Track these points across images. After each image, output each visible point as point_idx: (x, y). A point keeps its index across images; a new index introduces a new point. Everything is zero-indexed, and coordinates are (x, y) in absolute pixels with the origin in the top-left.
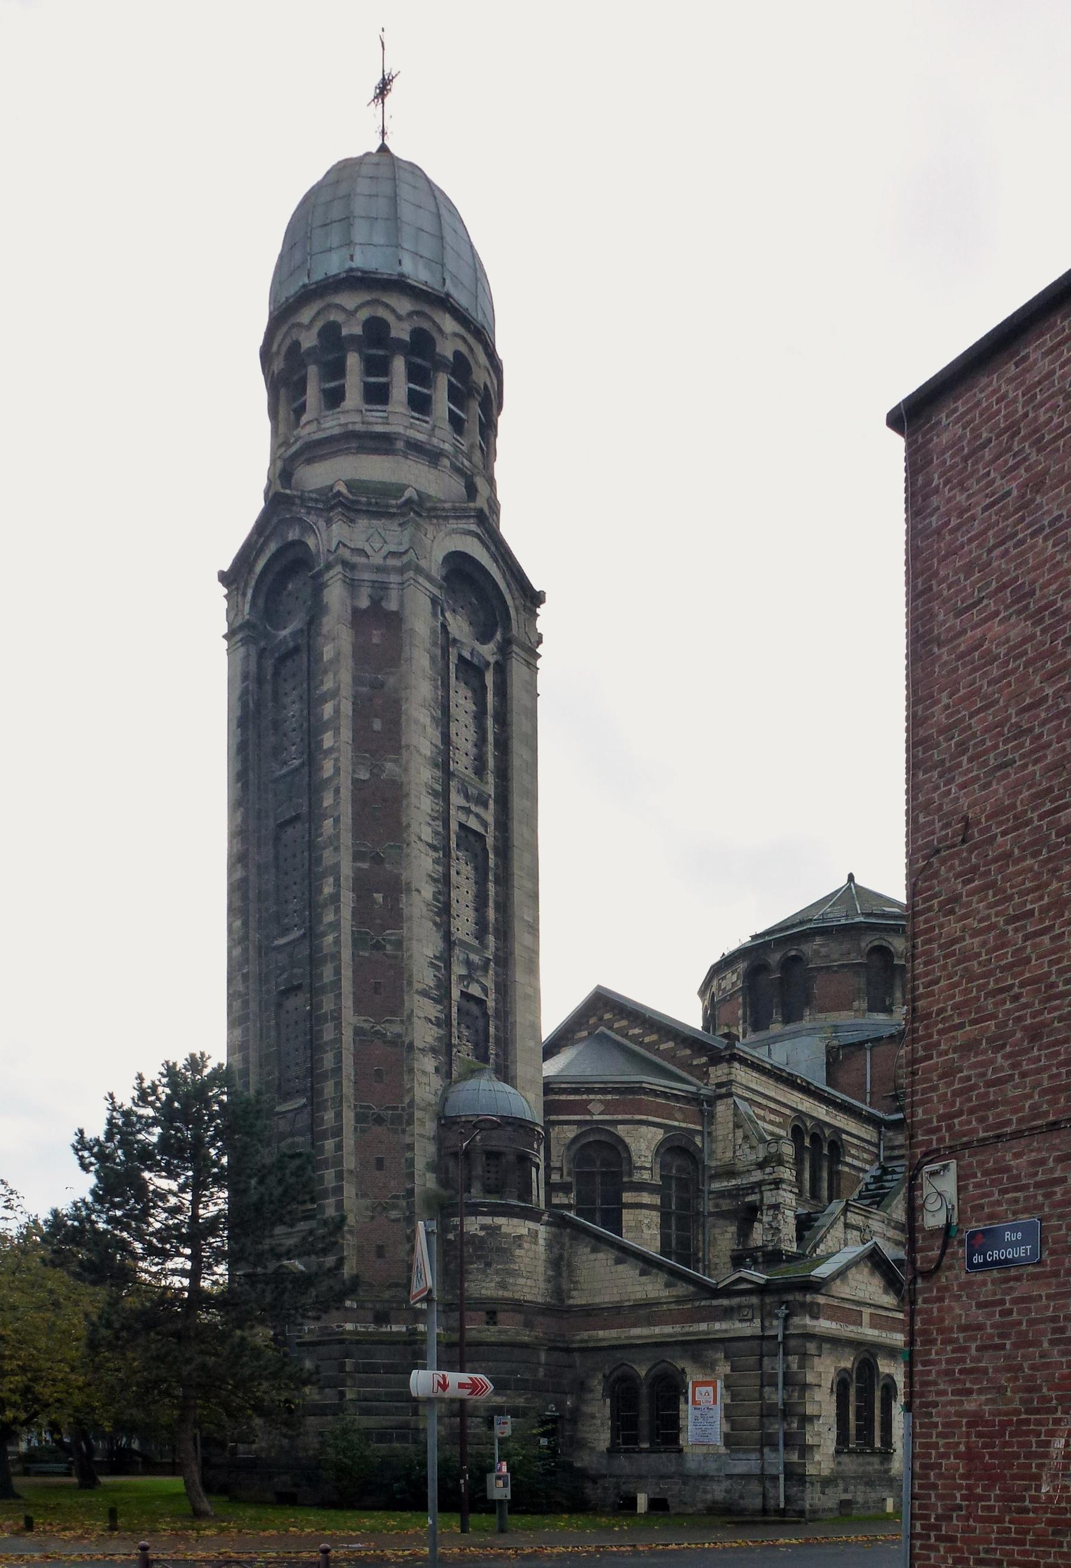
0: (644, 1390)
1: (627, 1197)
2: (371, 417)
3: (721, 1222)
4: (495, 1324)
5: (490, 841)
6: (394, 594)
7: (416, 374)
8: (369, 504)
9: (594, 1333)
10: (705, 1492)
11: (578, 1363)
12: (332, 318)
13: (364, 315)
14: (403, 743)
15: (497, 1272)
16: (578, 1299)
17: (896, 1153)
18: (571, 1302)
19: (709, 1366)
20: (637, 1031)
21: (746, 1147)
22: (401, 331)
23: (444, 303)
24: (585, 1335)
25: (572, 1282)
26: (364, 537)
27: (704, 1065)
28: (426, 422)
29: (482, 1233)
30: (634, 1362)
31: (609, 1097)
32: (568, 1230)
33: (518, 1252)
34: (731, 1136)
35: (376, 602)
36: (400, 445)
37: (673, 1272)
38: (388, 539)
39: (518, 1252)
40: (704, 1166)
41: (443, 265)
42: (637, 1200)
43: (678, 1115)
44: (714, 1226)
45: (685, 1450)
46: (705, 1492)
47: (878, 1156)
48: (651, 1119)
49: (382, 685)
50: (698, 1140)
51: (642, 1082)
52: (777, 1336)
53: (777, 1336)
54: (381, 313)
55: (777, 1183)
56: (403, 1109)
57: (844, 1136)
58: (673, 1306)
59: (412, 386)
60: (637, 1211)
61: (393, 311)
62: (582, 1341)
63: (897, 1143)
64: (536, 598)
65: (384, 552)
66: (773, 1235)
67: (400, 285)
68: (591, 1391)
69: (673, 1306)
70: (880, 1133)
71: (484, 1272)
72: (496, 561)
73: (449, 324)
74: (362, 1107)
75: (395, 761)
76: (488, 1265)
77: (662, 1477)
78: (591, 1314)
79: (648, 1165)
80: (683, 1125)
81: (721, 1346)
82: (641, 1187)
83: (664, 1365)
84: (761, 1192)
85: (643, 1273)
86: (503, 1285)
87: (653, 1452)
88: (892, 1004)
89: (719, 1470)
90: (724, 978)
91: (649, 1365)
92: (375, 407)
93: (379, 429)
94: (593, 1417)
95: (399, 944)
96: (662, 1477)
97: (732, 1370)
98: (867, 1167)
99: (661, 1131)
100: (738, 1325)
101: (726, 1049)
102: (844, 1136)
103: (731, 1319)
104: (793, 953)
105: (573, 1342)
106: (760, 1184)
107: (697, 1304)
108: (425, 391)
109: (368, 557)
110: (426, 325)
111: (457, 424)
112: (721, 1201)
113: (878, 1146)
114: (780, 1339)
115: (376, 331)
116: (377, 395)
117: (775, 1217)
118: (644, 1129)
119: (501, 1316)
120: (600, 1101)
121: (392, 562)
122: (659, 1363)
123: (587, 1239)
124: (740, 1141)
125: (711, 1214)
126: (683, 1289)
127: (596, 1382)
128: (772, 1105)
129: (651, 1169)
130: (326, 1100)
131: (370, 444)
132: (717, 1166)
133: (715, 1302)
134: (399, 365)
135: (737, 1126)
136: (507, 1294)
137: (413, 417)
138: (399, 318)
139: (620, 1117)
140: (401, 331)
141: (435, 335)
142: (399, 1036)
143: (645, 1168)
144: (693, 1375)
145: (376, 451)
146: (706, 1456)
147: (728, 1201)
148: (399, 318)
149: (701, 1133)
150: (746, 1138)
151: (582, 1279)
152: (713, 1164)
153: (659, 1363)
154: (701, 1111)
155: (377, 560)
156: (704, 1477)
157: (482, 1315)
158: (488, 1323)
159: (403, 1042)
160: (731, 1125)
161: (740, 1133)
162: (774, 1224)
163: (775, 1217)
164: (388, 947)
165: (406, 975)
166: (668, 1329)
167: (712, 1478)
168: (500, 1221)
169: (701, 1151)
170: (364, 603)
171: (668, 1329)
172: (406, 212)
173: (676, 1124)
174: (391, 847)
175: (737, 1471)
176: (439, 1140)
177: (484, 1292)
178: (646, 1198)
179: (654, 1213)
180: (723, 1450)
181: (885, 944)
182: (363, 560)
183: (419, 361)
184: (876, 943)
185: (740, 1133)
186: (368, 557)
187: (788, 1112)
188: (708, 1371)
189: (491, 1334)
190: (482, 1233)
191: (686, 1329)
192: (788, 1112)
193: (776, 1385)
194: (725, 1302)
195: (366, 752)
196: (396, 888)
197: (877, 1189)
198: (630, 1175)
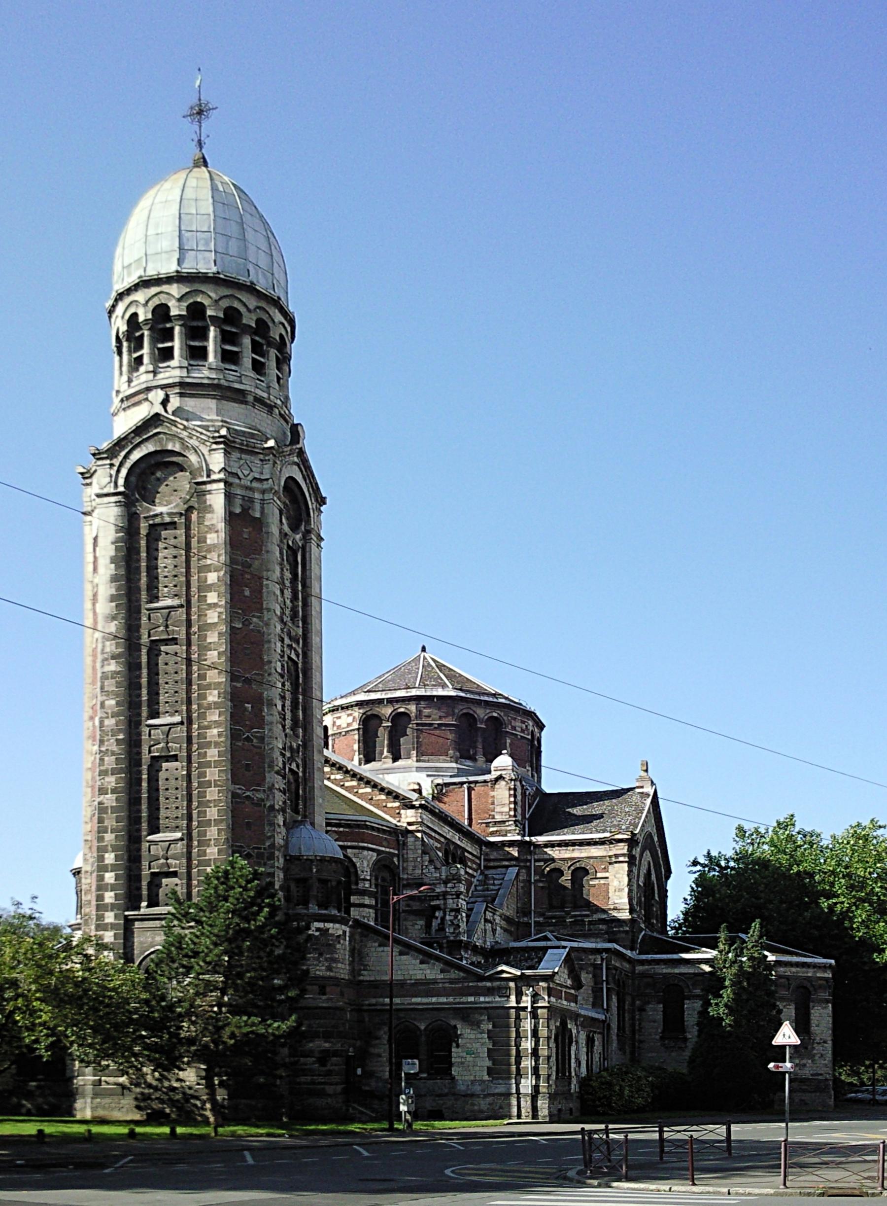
0: (423, 1038)
1: (354, 899)
2: (231, 376)
3: (412, 917)
4: (324, 994)
5: (300, 665)
6: (257, 506)
7: (256, 348)
8: (242, 444)
9: (381, 1000)
10: (473, 1105)
11: (367, 1019)
12: (199, 300)
13: (225, 303)
14: (264, 606)
15: (326, 959)
16: (366, 976)
17: (492, 864)
18: (361, 978)
19: (476, 1025)
20: (339, 777)
21: (431, 868)
22: (250, 320)
23: (276, 303)
24: (373, 1001)
25: (362, 965)
26: (237, 465)
27: (398, 808)
28: (262, 381)
29: (317, 934)
30: (415, 1019)
31: (341, 829)
32: (359, 930)
33: (338, 946)
34: (419, 859)
35: (245, 510)
36: (250, 398)
37: (447, 963)
38: (254, 469)
39: (338, 946)
40: (399, 878)
41: (273, 274)
42: (361, 901)
43: (385, 843)
44: (405, 920)
45: (457, 1078)
46: (473, 1105)
47: (480, 865)
48: (370, 846)
49: (250, 566)
50: (395, 860)
51: (365, 821)
52: (527, 1007)
53: (527, 1007)
54: (236, 305)
55: (458, 895)
56: (265, 849)
57: (466, 854)
58: (447, 985)
59: (254, 356)
60: (361, 909)
61: (245, 305)
62: (370, 1005)
63: (492, 857)
64: (322, 501)
65: (250, 478)
66: (455, 929)
67: (251, 289)
68: (377, 1038)
69: (447, 985)
70: (481, 850)
71: (318, 959)
72: (305, 480)
73: (278, 317)
74: (237, 846)
75: (258, 617)
76: (321, 954)
77: (440, 1095)
78: (376, 987)
79: (368, 878)
80: (388, 850)
81: (485, 1011)
82: (363, 893)
83: (439, 1022)
84: (445, 899)
85: (422, 962)
86: (329, 969)
87: (430, 1079)
88: (475, 754)
89: (483, 1091)
90: (339, 718)
91: (428, 1022)
92: (227, 366)
93: (237, 386)
94: (379, 1056)
95: (262, 739)
96: (440, 1095)
97: (494, 1027)
98: (475, 874)
99: (375, 854)
100: (498, 999)
101: (416, 800)
102: (466, 854)
103: (493, 995)
104: (402, 710)
105: (363, 1005)
106: (445, 894)
107: (466, 984)
108: (262, 360)
109: (240, 479)
110: (265, 317)
111: (258, 367)
112: (411, 902)
113: (480, 859)
114: (529, 1009)
115: (231, 316)
116: (229, 357)
117: (456, 917)
118: (365, 853)
119: (328, 989)
120: (335, 831)
121: (255, 485)
122: (437, 1021)
123: (376, 937)
124: (426, 863)
125: (404, 911)
126: (454, 974)
127: (382, 1032)
128: (437, 836)
129: (370, 880)
130: (210, 840)
131: (229, 394)
132: (408, 879)
133: (480, 984)
134: (247, 341)
135: (424, 852)
136: (332, 974)
137: (258, 379)
138: (249, 310)
139: (349, 844)
140: (250, 320)
141: (271, 324)
142: (263, 800)
143: (367, 880)
144: (465, 1032)
145: (234, 400)
146: (473, 1082)
147: (418, 904)
148: (249, 310)
149: (398, 856)
150: (431, 861)
151: (370, 963)
152: (405, 876)
153: (437, 1021)
154: (398, 841)
155: (246, 482)
156: (472, 1095)
157: (316, 988)
158: (319, 994)
159: (265, 805)
160: (420, 851)
161: (427, 858)
162: (455, 922)
163: (456, 917)
164: (255, 741)
165: (267, 760)
166: (443, 1000)
167: (478, 1096)
168: (329, 925)
169: (398, 867)
170: (238, 510)
171: (443, 1000)
172: (250, 235)
173: (383, 849)
174: (255, 674)
175: (497, 1091)
176: (286, 870)
177: (318, 973)
178: (367, 901)
179: (371, 910)
180: (486, 1078)
181: (471, 712)
182: (237, 481)
183: (257, 338)
184: (464, 711)
185: (427, 858)
186: (240, 479)
187: (442, 840)
188: (475, 1027)
189: (323, 1001)
190: (317, 934)
191: (458, 1000)
192: (442, 840)
193: (527, 1037)
194: (489, 984)
195: (239, 609)
196: (259, 701)
197: (483, 891)
198: (357, 884)
